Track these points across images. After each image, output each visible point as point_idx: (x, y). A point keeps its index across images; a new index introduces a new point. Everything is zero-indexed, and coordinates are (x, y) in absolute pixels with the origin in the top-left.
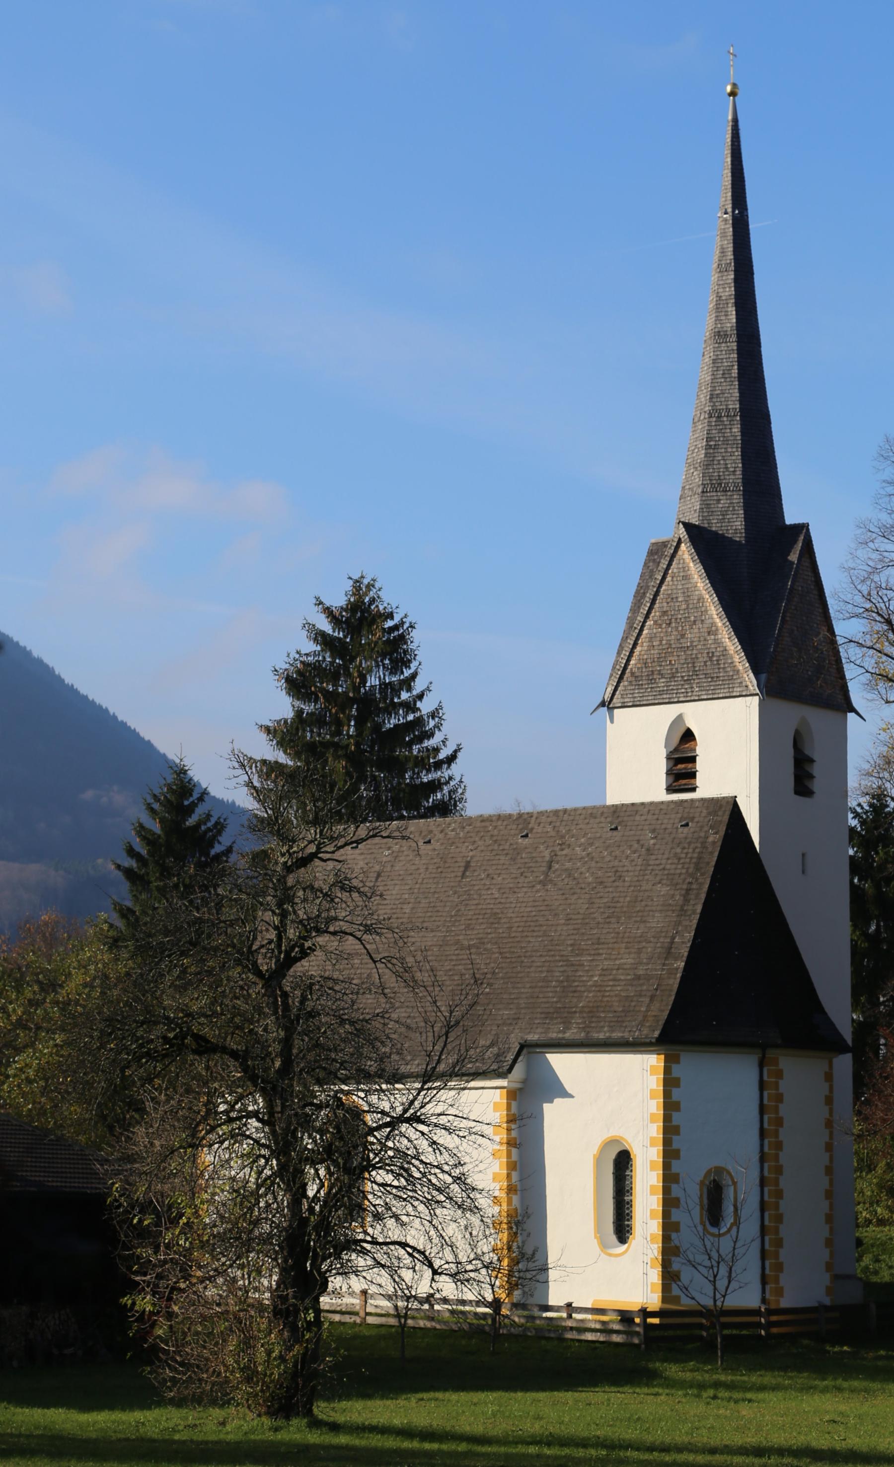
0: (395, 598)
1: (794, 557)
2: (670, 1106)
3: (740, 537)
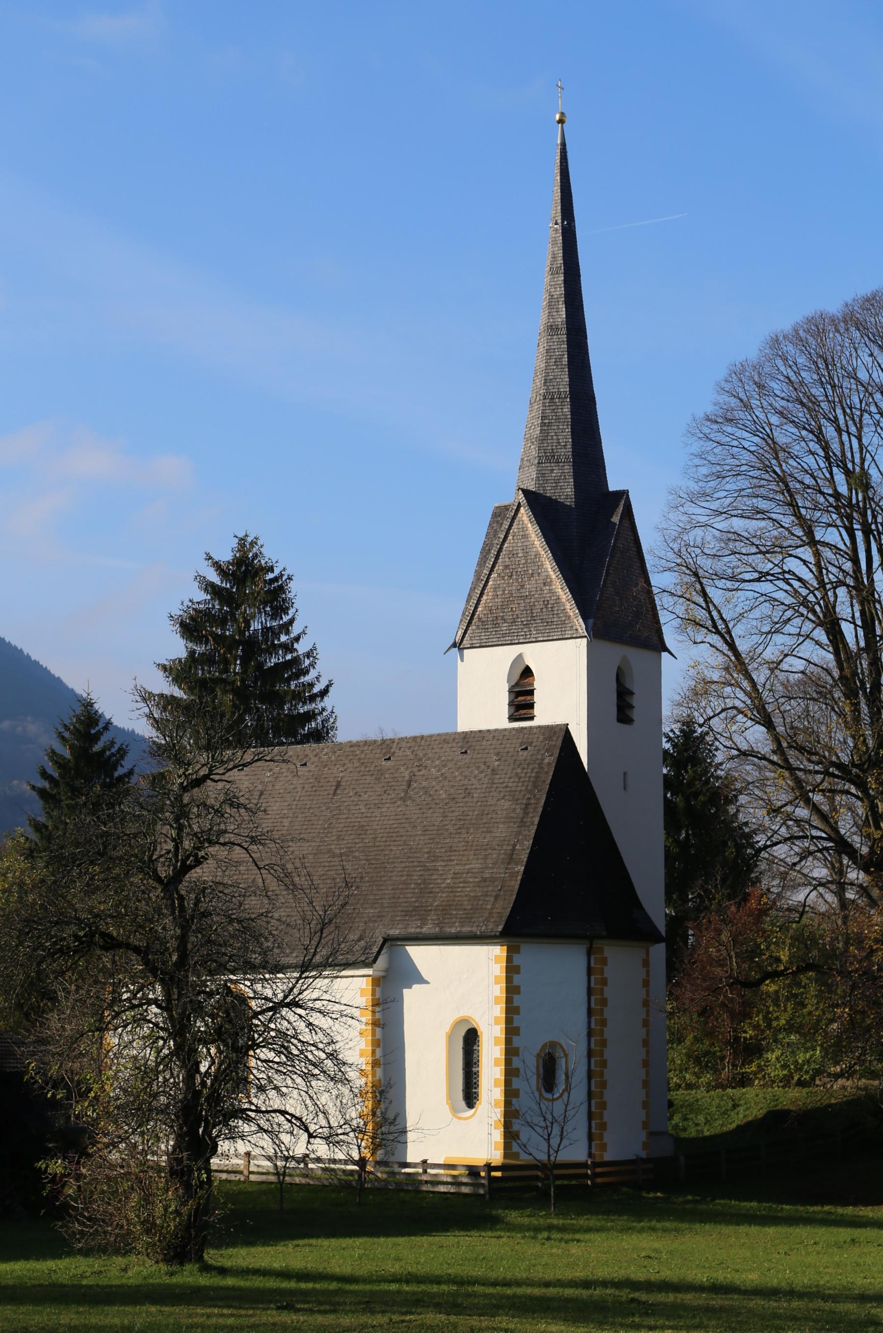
0: (275, 553)
1: (616, 519)
2: (512, 990)
3: (570, 502)
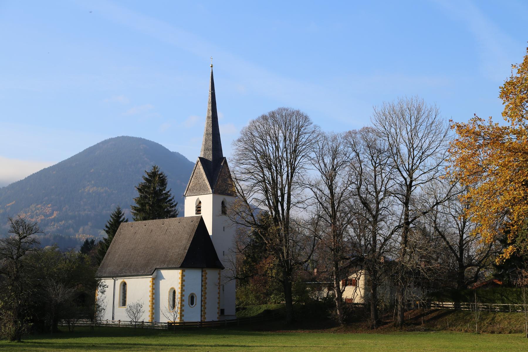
2: (183, 281)
